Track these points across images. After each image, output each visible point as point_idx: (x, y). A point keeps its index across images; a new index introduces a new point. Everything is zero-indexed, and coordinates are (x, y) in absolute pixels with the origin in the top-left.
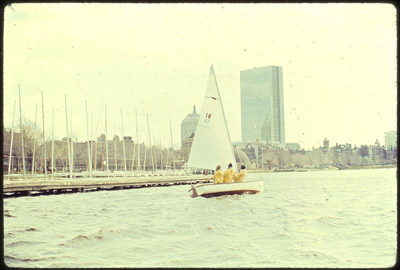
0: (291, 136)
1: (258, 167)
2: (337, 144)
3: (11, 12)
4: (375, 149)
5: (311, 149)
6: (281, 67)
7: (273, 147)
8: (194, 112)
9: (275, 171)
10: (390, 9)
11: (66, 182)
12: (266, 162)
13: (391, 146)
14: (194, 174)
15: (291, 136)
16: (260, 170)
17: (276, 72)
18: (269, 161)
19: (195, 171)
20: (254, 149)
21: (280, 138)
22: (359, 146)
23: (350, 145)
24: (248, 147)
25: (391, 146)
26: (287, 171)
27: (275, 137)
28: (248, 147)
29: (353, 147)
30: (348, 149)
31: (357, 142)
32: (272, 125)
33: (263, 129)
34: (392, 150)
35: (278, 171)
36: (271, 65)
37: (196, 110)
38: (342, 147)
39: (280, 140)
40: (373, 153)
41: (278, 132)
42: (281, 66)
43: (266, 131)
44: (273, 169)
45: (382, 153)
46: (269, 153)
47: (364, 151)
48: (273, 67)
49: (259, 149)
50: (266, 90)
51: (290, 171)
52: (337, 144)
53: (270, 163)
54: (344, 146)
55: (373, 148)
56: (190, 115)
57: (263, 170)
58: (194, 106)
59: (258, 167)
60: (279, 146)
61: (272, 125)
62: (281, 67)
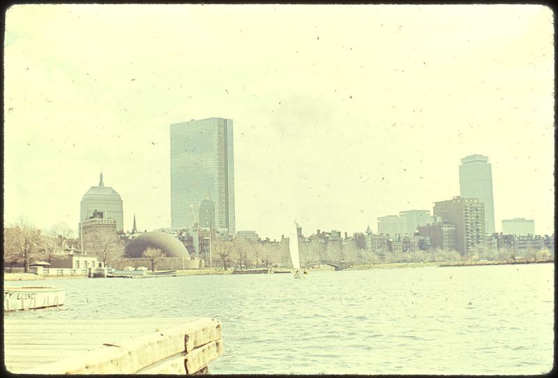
0: (244, 220)
1: (203, 265)
2: (319, 231)
3: (14, 14)
4: (375, 239)
5: (279, 240)
6: (231, 121)
7: (222, 234)
8: (101, 183)
9: (235, 272)
10: (544, 13)
11: (280, 271)
12: (218, 257)
13: (399, 235)
14: (90, 276)
15: (244, 220)
16: (207, 270)
17: (224, 126)
18: (223, 256)
19: (93, 272)
20: (192, 238)
21: (227, 223)
22: (351, 235)
23: (339, 233)
24: (183, 235)
25: (399, 235)
26: (255, 272)
27: (221, 222)
28: (183, 235)
29: (343, 236)
30: (335, 238)
31: (351, 228)
32: (217, 205)
33: (202, 211)
34: (399, 240)
35: (240, 273)
36: (217, 117)
37: (104, 181)
38: (327, 235)
39: (227, 226)
40: (372, 245)
41: (224, 215)
42: (231, 118)
43: (206, 211)
44: (230, 270)
45: (25, 265)
46: (212, 245)
47: (359, 241)
48: (219, 119)
49: (199, 238)
50: (207, 151)
51: (261, 272)
52: (319, 231)
53: (226, 258)
54: (330, 234)
55: (374, 238)
56: (93, 188)
57: (212, 270)
58: (101, 175)
59: (203, 265)
60: (231, 234)
61: (217, 205)
62: (231, 121)
